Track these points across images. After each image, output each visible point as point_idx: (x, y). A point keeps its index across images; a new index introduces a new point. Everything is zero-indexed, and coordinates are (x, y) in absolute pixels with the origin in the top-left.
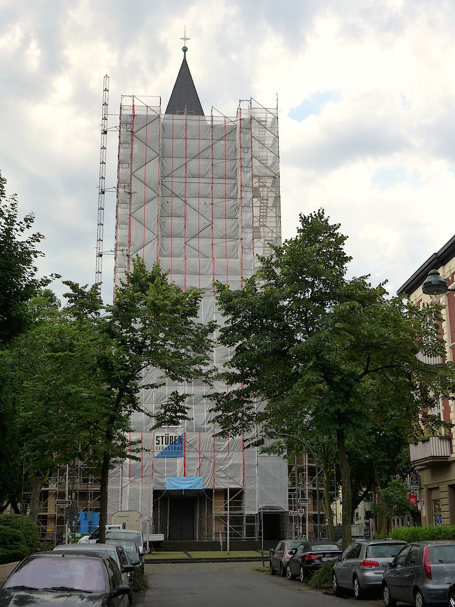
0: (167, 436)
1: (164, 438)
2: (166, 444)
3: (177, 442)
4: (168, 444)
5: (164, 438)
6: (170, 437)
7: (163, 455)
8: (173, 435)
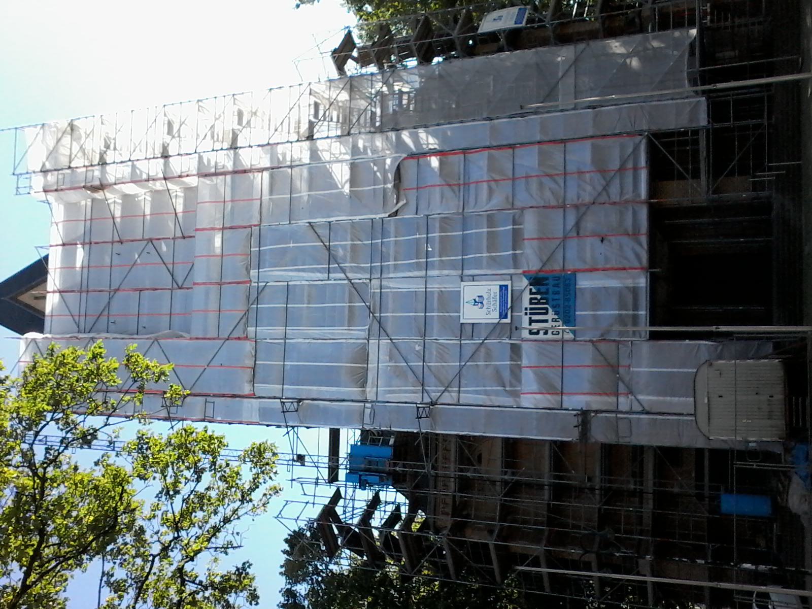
0: (528, 311)
1: (534, 317)
2: (546, 313)
3: (543, 289)
4: (547, 309)
5: (534, 317)
6: (531, 303)
7: (568, 318)
8: (526, 297)
